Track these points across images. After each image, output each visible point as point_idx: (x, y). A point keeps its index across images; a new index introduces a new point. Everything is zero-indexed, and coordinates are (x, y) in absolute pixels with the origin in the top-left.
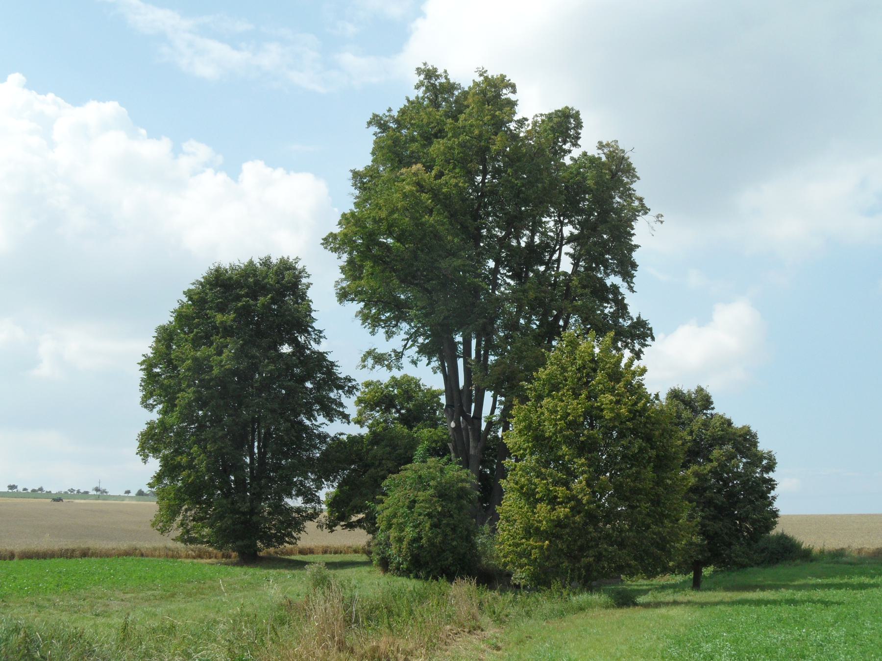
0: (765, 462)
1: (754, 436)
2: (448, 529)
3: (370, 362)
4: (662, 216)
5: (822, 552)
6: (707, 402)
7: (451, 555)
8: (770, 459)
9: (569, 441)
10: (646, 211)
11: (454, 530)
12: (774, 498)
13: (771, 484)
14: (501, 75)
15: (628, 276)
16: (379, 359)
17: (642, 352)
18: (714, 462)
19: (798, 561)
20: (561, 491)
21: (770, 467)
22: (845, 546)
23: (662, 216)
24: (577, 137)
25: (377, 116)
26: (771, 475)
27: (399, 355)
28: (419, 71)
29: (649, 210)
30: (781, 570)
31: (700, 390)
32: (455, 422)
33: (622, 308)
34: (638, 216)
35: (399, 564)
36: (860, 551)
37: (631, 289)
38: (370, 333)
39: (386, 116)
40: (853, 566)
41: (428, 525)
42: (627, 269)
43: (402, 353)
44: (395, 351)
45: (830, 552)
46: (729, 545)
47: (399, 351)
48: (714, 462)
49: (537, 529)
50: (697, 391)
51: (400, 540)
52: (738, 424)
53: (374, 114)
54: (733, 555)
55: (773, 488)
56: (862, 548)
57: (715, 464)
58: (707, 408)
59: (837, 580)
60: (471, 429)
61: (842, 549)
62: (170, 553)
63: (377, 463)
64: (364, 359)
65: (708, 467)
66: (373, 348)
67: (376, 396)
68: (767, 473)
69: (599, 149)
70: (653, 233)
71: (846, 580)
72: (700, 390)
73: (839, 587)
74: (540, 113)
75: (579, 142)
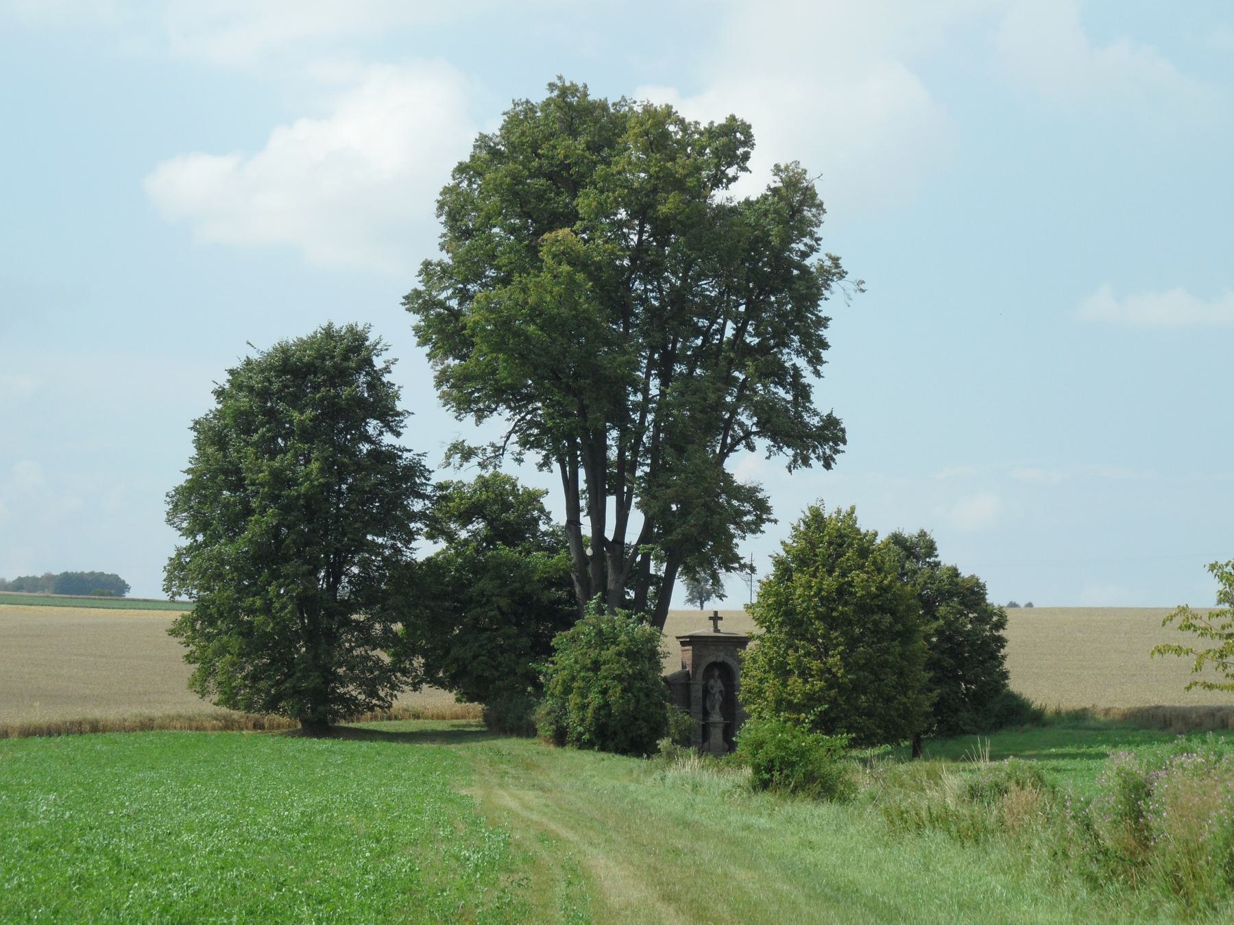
0: (995, 619)
1: (983, 587)
2: (642, 695)
3: (457, 458)
4: (863, 282)
5: (1058, 713)
6: (931, 548)
7: (645, 724)
8: (1001, 616)
9: (820, 617)
10: (842, 275)
11: (647, 695)
12: (1004, 657)
13: (1001, 642)
14: (667, 106)
15: (816, 361)
16: (467, 454)
17: (834, 460)
18: (941, 620)
19: (1027, 726)
20: (815, 665)
21: (1000, 625)
22: (1088, 705)
23: (863, 282)
24: (746, 157)
25: (486, 136)
26: (1001, 632)
27: (499, 451)
28: (552, 86)
29: (846, 273)
30: (1008, 737)
31: (923, 534)
32: (592, 549)
33: (802, 393)
34: (832, 280)
35: (581, 734)
36: (1107, 712)
37: (817, 373)
38: (456, 418)
39: (497, 137)
40: (1096, 732)
41: (618, 689)
42: (814, 348)
43: (504, 448)
44: (493, 445)
45: (1068, 714)
46: (956, 711)
47: (498, 445)
48: (941, 620)
49: (790, 702)
50: (919, 536)
51: (584, 707)
52: (965, 573)
53: (481, 134)
54: (961, 723)
55: (1003, 647)
56: (911, 760)
57: (942, 622)
58: (930, 556)
59: (1072, 750)
60: (610, 557)
61: (1084, 710)
62: (194, 724)
63: (484, 600)
64: (448, 457)
65: (935, 625)
66: (460, 440)
67: (462, 504)
68: (998, 631)
69: (775, 175)
70: (849, 302)
71: (1083, 750)
72: (923, 534)
73: (1073, 756)
74: (695, 120)
75: (748, 164)
